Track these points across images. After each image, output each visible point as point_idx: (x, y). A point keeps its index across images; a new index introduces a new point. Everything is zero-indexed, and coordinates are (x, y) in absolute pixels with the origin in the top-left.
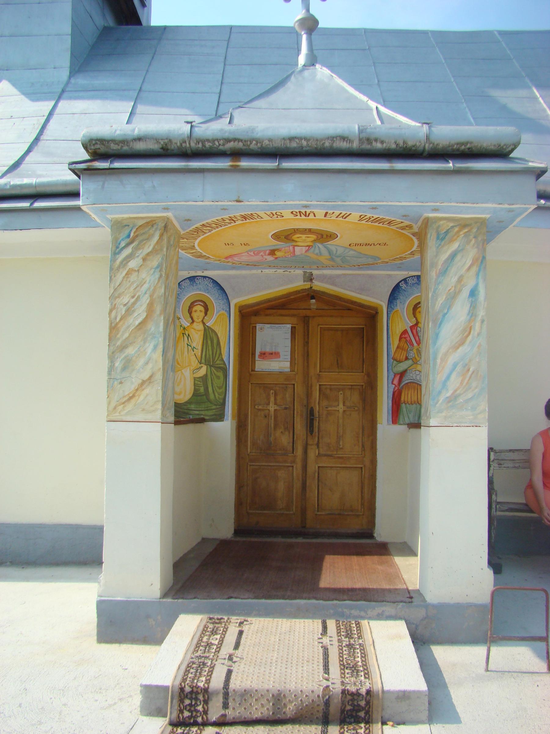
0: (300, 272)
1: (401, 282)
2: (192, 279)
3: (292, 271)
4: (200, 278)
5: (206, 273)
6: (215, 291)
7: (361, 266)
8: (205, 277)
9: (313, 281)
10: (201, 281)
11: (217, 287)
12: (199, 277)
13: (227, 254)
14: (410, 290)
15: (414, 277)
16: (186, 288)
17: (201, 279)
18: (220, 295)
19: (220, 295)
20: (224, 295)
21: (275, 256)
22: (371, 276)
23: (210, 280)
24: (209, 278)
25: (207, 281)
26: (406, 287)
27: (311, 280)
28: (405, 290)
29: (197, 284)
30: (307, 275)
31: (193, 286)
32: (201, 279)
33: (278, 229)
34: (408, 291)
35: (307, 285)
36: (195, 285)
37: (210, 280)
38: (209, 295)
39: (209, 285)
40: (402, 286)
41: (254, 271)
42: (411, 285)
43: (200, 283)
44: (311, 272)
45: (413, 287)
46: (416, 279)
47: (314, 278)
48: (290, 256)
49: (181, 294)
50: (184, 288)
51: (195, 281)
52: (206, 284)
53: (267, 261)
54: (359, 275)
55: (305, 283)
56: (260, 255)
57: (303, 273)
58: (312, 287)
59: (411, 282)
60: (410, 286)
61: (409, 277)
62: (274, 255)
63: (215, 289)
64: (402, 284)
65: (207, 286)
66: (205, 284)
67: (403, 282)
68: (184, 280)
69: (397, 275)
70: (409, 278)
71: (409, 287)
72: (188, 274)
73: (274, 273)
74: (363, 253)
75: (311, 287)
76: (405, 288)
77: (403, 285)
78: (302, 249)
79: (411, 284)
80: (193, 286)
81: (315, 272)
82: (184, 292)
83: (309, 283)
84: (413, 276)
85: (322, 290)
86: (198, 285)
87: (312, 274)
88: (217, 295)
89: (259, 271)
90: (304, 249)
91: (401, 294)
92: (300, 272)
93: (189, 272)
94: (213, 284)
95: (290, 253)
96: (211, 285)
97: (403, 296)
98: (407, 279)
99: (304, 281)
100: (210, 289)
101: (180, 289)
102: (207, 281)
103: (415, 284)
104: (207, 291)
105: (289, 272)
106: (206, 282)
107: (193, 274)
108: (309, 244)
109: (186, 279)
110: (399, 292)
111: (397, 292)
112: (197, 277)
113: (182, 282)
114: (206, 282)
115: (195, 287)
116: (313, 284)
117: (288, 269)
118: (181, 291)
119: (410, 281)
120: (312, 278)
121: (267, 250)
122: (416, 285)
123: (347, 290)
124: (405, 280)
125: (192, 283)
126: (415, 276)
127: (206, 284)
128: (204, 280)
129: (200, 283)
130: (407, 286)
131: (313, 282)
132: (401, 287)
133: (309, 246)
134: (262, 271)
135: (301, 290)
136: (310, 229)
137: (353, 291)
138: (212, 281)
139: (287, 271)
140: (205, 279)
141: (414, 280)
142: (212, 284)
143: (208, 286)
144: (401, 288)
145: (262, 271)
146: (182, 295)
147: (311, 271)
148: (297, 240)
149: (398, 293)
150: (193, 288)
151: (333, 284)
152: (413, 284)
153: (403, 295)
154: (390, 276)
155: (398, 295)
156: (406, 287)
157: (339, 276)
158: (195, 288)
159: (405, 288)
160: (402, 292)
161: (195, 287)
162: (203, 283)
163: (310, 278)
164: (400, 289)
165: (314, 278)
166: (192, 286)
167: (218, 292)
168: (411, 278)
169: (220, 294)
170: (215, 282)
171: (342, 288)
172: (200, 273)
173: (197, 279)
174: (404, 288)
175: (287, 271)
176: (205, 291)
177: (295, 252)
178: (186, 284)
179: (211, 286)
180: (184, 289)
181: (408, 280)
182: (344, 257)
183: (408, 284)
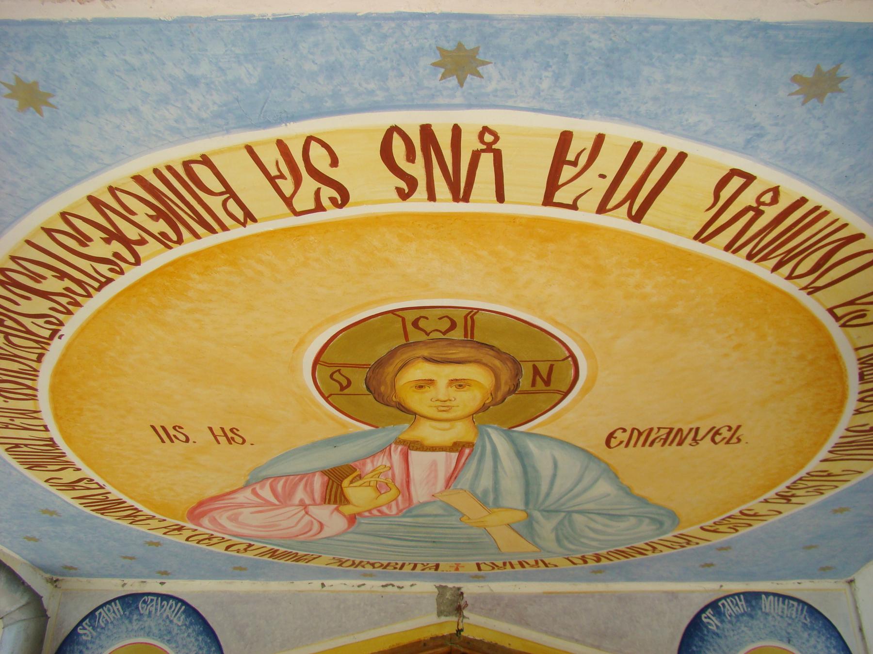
0: (427, 587)
1: (703, 610)
2: (130, 601)
3: (406, 584)
4: (152, 600)
5: (172, 587)
6: (189, 636)
7: (604, 562)
8: (166, 597)
9: (465, 613)
10: (153, 609)
11: (197, 628)
12: (150, 597)
13: (190, 497)
14: (732, 633)
15: (737, 597)
16: (110, 626)
17: (154, 603)
18: (201, 648)
19: (201, 648)
20: (213, 649)
21: (348, 510)
22: (622, 598)
23: (180, 604)
24: (178, 600)
25: (171, 607)
26: (719, 624)
27: (459, 610)
28: (717, 635)
29: (141, 615)
30: (448, 596)
31: (131, 622)
32: (154, 603)
33: (334, 319)
34: (725, 636)
35: (448, 626)
36: (135, 617)
37: (180, 604)
38: (172, 648)
39: (175, 620)
40: (708, 623)
41: (302, 585)
42: (734, 620)
43: (150, 612)
44: (459, 589)
45: (738, 624)
46: (743, 602)
47: (467, 605)
48: (394, 511)
49: (94, 643)
50: (103, 625)
51: (137, 608)
52: (167, 617)
53: (328, 538)
54: (592, 594)
55: (443, 619)
56: (296, 501)
57: (436, 590)
58: (462, 630)
59: (730, 611)
60: (730, 622)
61: (725, 598)
62: (341, 503)
63: (190, 631)
64: (708, 617)
65: (168, 622)
66: (164, 616)
67: (710, 610)
68: (109, 602)
69: (693, 592)
70: (723, 601)
71: (727, 626)
72: (120, 588)
73: (358, 591)
74: (637, 491)
75: (459, 631)
76: (717, 627)
77: (711, 620)
78: (434, 464)
79: (730, 616)
80: (131, 622)
81: (470, 588)
82: (103, 637)
83: (454, 619)
84: (728, 596)
85: (489, 638)
86: (145, 618)
87: (462, 593)
88: (194, 648)
89: (317, 584)
90: (444, 461)
91: (709, 647)
92: (427, 587)
93: (126, 581)
94: (188, 616)
95: (393, 492)
96: (180, 620)
97: (715, 650)
98: (720, 604)
99: (440, 613)
100: (176, 630)
101: (94, 628)
102: (171, 607)
103: (742, 615)
104: (167, 638)
105: (399, 587)
106: (168, 612)
107: (134, 586)
108: (461, 431)
109: (114, 600)
110: (702, 640)
111: (697, 639)
112: (146, 597)
113: (101, 610)
114: (168, 610)
115: (134, 623)
116: (465, 620)
117: (397, 579)
118: (95, 634)
119: (729, 609)
120: (462, 603)
121: (314, 474)
122: (745, 618)
123: (558, 636)
124: (714, 605)
125: (127, 613)
126: (738, 594)
127: (167, 617)
128: (162, 607)
129: (150, 612)
130: (722, 622)
131: (464, 617)
132: (706, 625)
133: (458, 447)
134: (323, 585)
135: (432, 638)
136: (472, 313)
137: (577, 641)
138: (184, 607)
139: (393, 585)
140: (165, 603)
141: (737, 605)
142: (183, 616)
143: (171, 622)
144: (707, 627)
145: (323, 585)
146: (95, 647)
147: (457, 585)
148: (416, 401)
149: (700, 643)
150: (130, 626)
151: (522, 620)
152: (737, 617)
153: (716, 647)
154: (673, 595)
155: (701, 647)
156: (719, 624)
157: (534, 598)
158: (136, 628)
159: (717, 627)
160: (711, 640)
161: (135, 626)
162: (158, 614)
163: (456, 605)
164: (706, 632)
165: (467, 605)
166: (127, 622)
167: (197, 640)
168: (728, 600)
169: (203, 645)
170: (191, 612)
171: (546, 632)
172: (153, 586)
173: (145, 602)
174: (714, 628)
175: (393, 585)
176: (161, 637)
177: (412, 488)
178: (112, 615)
179: (180, 623)
180: (103, 628)
181: (723, 605)
182: (569, 513)
183: (724, 618)
